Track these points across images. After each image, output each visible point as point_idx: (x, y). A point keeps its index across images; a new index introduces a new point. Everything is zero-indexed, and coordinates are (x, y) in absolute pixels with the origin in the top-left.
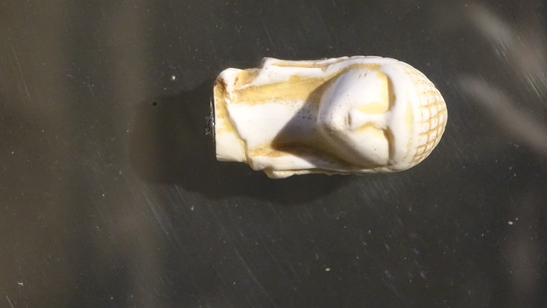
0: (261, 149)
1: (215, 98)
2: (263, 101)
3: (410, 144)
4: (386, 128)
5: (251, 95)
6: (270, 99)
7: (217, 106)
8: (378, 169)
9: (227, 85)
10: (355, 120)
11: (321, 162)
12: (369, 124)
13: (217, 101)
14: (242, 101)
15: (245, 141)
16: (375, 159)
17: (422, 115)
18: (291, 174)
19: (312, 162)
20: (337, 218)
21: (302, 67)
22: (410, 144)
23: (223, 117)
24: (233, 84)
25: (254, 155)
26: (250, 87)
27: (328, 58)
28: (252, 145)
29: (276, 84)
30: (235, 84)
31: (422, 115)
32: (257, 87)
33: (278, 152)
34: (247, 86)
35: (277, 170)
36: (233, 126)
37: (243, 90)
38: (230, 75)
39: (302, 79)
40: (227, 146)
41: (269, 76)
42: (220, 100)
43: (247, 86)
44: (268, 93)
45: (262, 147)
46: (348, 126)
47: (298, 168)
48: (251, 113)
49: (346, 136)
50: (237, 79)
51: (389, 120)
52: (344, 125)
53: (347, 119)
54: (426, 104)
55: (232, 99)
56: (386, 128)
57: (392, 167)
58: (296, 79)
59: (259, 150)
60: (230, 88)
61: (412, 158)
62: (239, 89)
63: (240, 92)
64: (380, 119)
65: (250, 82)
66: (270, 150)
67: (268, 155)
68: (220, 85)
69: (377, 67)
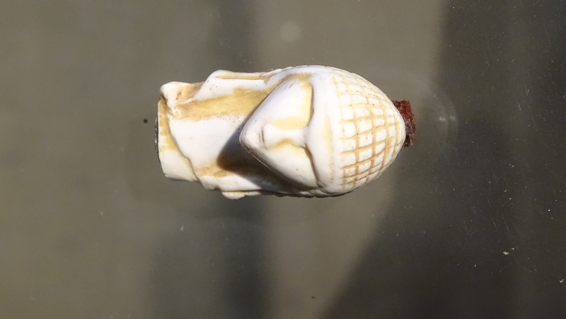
0: (208, 168)
1: (159, 114)
2: (208, 116)
3: (332, 165)
4: (304, 146)
5: (195, 109)
6: (216, 114)
7: (161, 123)
8: (313, 191)
9: (167, 100)
10: (267, 137)
11: (264, 183)
12: (285, 142)
13: (161, 117)
14: (188, 116)
15: (189, 160)
16: (300, 179)
17: (343, 130)
18: (241, 195)
19: (256, 182)
20: (397, 235)
21: (245, 79)
22: (333, 164)
23: (166, 134)
24: (175, 98)
25: (202, 175)
26: (193, 101)
27: (274, 70)
28: (196, 163)
29: (221, 98)
30: (177, 99)
31: (343, 130)
32: (201, 102)
33: (224, 171)
34: (190, 100)
35: (224, 191)
36: (175, 144)
37: (187, 105)
38: (170, 89)
39: (247, 92)
40: (171, 163)
41: (211, 89)
42: (163, 116)
43: (190, 100)
44: (215, 107)
45: (207, 166)
46: (262, 143)
47: (245, 189)
48: (192, 131)
49: (263, 155)
50: (180, 94)
51: (306, 136)
52: (258, 141)
53: (261, 136)
54: (351, 117)
55: (174, 114)
56: (304, 146)
57: (323, 189)
58: (240, 92)
59: (205, 170)
60: (172, 103)
61: (341, 180)
62: (182, 104)
63: (185, 108)
64: (296, 134)
65: (192, 97)
66: (217, 169)
67: (215, 174)
68: (163, 100)
69: (307, 77)
